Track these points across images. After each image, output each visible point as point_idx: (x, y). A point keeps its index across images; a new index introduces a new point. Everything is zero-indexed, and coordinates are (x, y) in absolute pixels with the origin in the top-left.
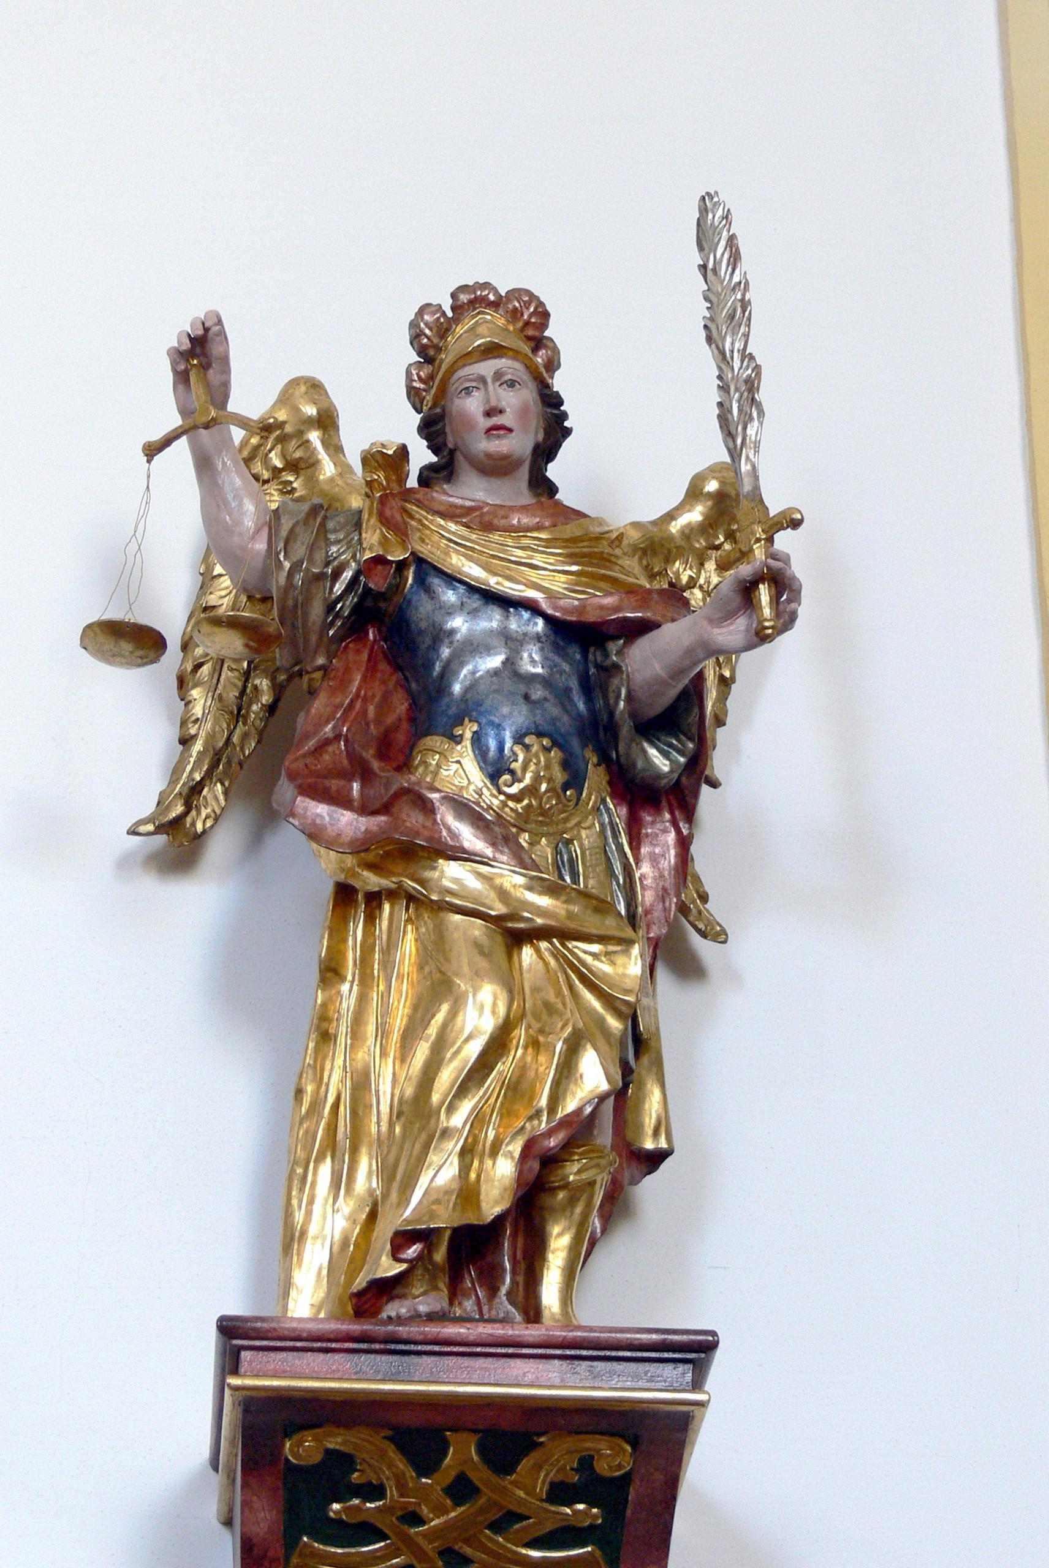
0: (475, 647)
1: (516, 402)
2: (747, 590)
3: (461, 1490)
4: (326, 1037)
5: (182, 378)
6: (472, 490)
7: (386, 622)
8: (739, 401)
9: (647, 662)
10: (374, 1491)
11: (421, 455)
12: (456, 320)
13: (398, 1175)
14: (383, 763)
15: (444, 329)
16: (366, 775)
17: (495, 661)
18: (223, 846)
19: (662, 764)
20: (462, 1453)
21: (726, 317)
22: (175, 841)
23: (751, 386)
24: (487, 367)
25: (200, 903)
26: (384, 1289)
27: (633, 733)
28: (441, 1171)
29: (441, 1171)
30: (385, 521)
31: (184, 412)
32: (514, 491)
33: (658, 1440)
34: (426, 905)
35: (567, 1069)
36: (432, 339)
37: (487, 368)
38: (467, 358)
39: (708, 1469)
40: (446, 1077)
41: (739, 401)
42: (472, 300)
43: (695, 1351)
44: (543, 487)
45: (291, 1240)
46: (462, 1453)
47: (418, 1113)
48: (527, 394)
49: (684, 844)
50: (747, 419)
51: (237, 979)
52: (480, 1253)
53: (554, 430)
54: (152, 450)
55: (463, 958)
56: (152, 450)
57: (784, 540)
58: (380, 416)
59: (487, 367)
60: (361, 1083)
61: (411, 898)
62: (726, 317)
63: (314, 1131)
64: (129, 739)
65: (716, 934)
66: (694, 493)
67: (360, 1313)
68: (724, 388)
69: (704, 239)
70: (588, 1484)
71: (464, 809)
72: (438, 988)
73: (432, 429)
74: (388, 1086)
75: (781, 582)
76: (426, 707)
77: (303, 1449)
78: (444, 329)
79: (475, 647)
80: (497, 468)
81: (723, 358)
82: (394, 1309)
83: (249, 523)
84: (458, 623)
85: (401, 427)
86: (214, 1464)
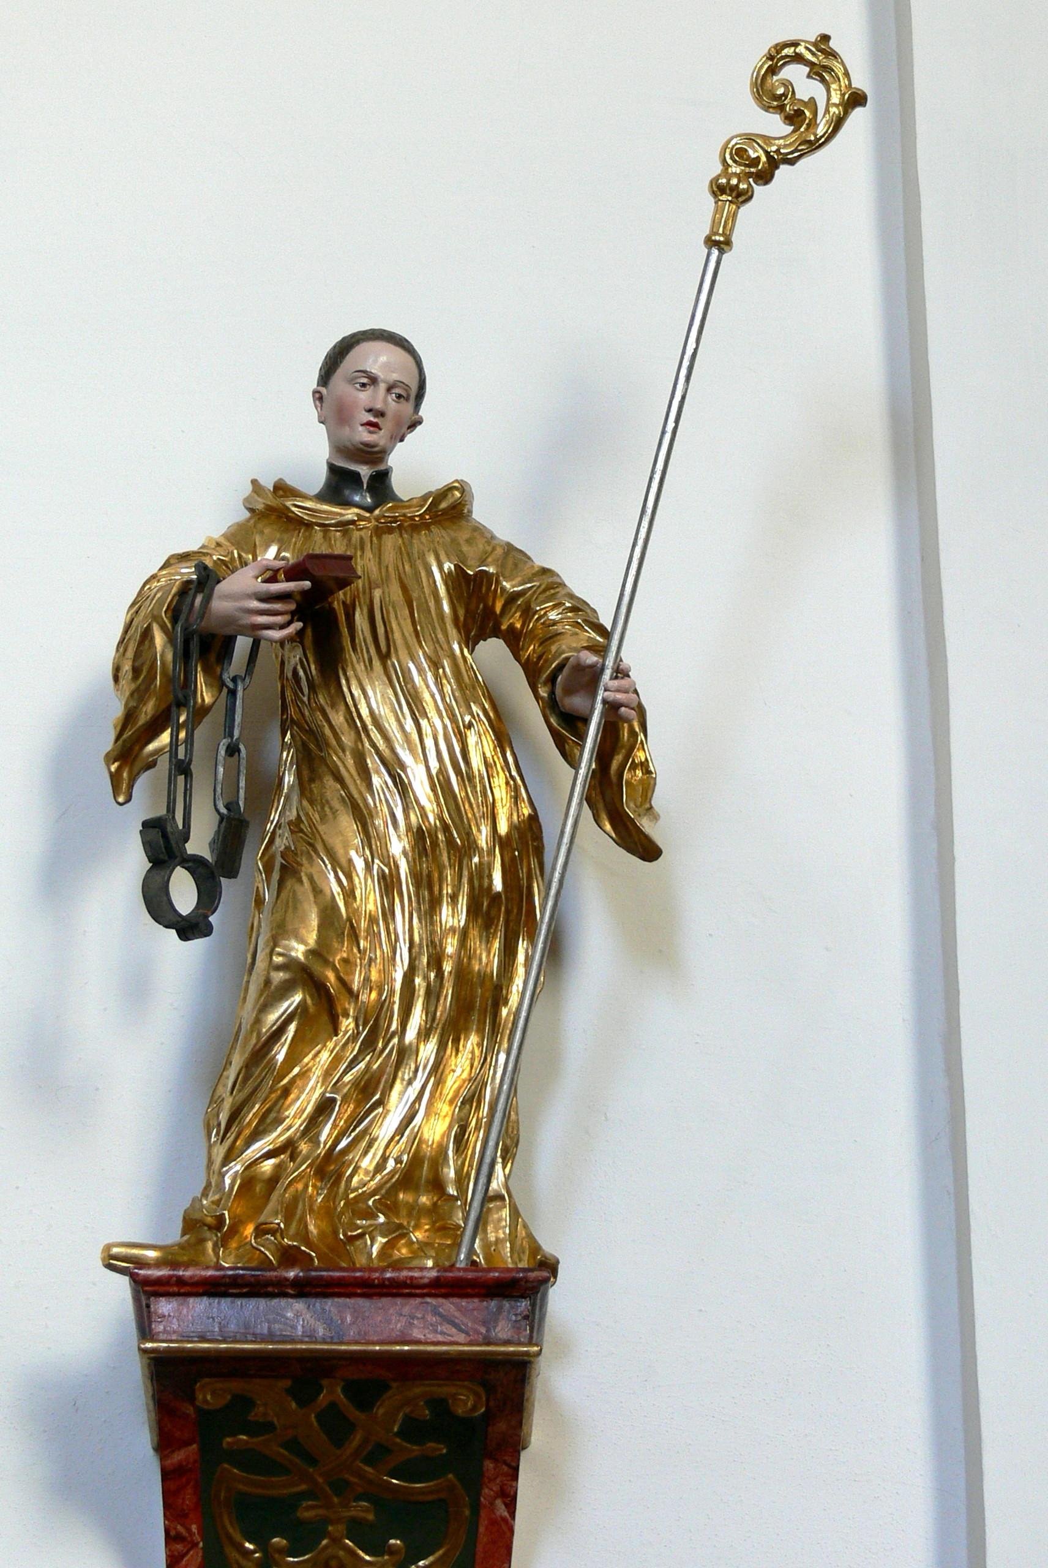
33: (506, 1385)
46: (332, 1393)
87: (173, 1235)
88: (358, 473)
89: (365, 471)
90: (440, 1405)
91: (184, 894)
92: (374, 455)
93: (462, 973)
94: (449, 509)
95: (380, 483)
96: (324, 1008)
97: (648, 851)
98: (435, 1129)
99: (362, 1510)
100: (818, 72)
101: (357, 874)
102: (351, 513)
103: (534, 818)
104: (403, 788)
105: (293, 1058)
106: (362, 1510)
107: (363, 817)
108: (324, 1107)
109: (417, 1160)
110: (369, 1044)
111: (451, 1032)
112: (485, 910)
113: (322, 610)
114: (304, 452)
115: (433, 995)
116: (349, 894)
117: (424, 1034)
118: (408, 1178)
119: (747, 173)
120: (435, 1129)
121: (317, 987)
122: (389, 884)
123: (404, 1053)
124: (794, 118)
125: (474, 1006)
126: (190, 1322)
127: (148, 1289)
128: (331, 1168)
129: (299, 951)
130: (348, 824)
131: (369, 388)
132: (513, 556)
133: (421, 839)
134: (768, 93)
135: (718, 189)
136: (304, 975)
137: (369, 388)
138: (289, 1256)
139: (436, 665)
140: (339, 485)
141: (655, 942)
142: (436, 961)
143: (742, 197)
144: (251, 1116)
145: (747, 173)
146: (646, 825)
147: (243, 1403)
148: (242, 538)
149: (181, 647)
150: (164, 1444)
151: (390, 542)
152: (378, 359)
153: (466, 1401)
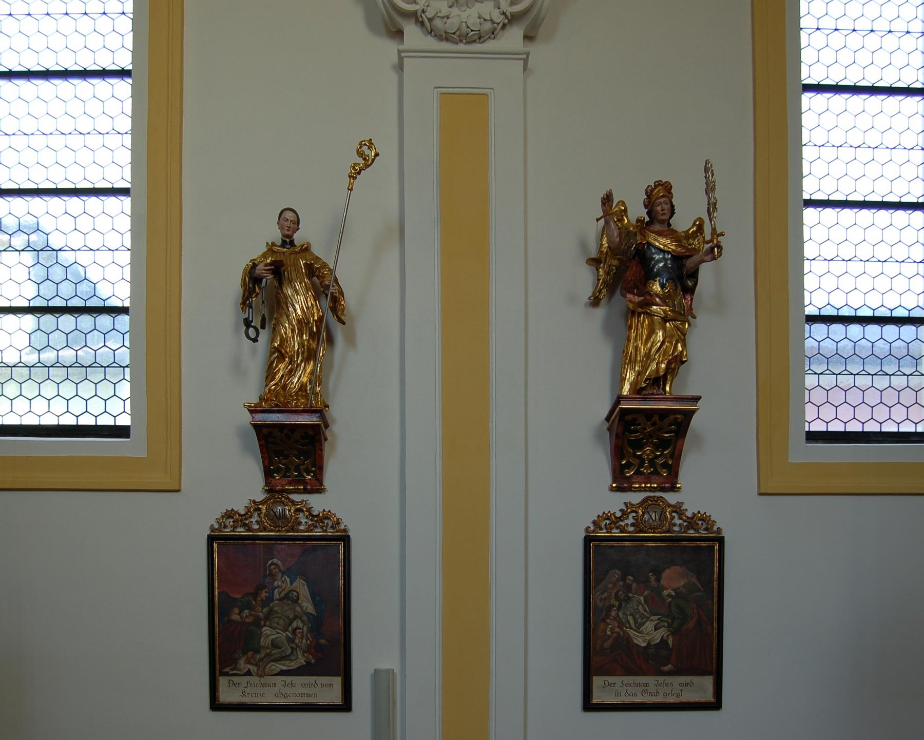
0: (659, 261)
1: (667, 207)
2: (712, 249)
3: (654, 424)
4: (629, 340)
5: (603, 204)
6: (657, 227)
7: (642, 256)
8: (712, 208)
9: (690, 263)
10: (639, 425)
11: (647, 219)
12: (655, 188)
13: (645, 368)
14: (641, 286)
15: (652, 191)
16: (638, 288)
17: (661, 265)
18: (603, 302)
19: (690, 284)
20: (656, 418)
21: (710, 188)
22: (595, 302)
23: (715, 204)
24: (659, 198)
25: (600, 313)
26: (643, 389)
27: (684, 276)
28: (653, 366)
29: (653, 366)
30: (641, 234)
31: (604, 211)
32: (665, 228)
33: (688, 415)
34: (650, 315)
35: (676, 347)
36: (649, 193)
37: (662, 200)
38: (658, 198)
39: (695, 421)
40: (653, 350)
41: (712, 208)
42: (658, 184)
43: (697, 399)
44: (669, 225)
45: (623, 380)
46: (656, 418)
47: (648, 355)
48: (669, 206)
49: (692, 300)
50: (714, 212)
51: (608, 328)
52: (658, 381)
53: (672, 213)
54: (598, 220)
55: (657, 326)
56: (598, 220)
57: (720, 238)
58: (637, 211)
59: (659, 198)
60: (636, 348)
61: (647, 313)
62: (710, 188)
63: (623, 359)
64: (585, 281)
65: (694, 317)
66: (694, 224)
67: (638, 394)
68: (709, 204)
69: (706, 170)
70: (676, 423)
71: (658, 295)
72: (652, 332)
73: (649, 213)
74: (643, 350)
75: (719, 247)
76: (649, 275)
77: (629, 418)
78: (652, 191)
79: (659, 261)
80: (662, 222)
81: (709, 199)
82: (644, 392)
83: (616, 234)
84: (657, 257)
85: (643, 213)
86: (608, 419)
87: (257, 401)
88: (288, 241)
89: (288, 240)
90: (676, 419)
91: (252, 332)
92: (290, 237)
93: (309, 349)
94: (306, 249)
95: (292, 243)
96: (281, 358)
97: (344, 323)
98: (305, 379)
99: (295, 452)
100: (369, 148)
101: (286, 329)
102: (285, 250)
103: (323, 316)
104: (295, 310)
105: (277, 366)
106: (295, 452)
107: (288, 317)
108: (283, 376)
109: (302, 386)
110: (290, 363)
111: (306, 360)
112: (312, 335)
113: (277, 269)
114: (276, 235)
115: (303, 353)
116: (286, 333)
117: (302, 362)
118: (300, 389)
119: (355, 174)
120: (305, 379)
121: (280, 352)
122: (293, 331)
123: (299, 365)
124: (365, 159)
125: (311, 355)
126: (261, 418)
127: (253, 411)
128: (284, 387)
129: (276, 345)
130: (285, 317)
131: (289, 221)
132: (317, 259)
133: (299, 321)
134: (360, 154)
135: (350, 177)
136: (277, 350)
137: (289, 221)
138: (277, 406)
139: (301, 283)
140: (284, 244)
141: (351, 341)
142: (303, 346)
143: (355, 178)
144: (270, 378)
145: (355, 174)
146: (343, 318)
147: (635, 420)
148: (264, 256)
149: (252, 279)
150: (259, 440)
151: (292, 256)
152: (289, 215)
153: (311, 432)
